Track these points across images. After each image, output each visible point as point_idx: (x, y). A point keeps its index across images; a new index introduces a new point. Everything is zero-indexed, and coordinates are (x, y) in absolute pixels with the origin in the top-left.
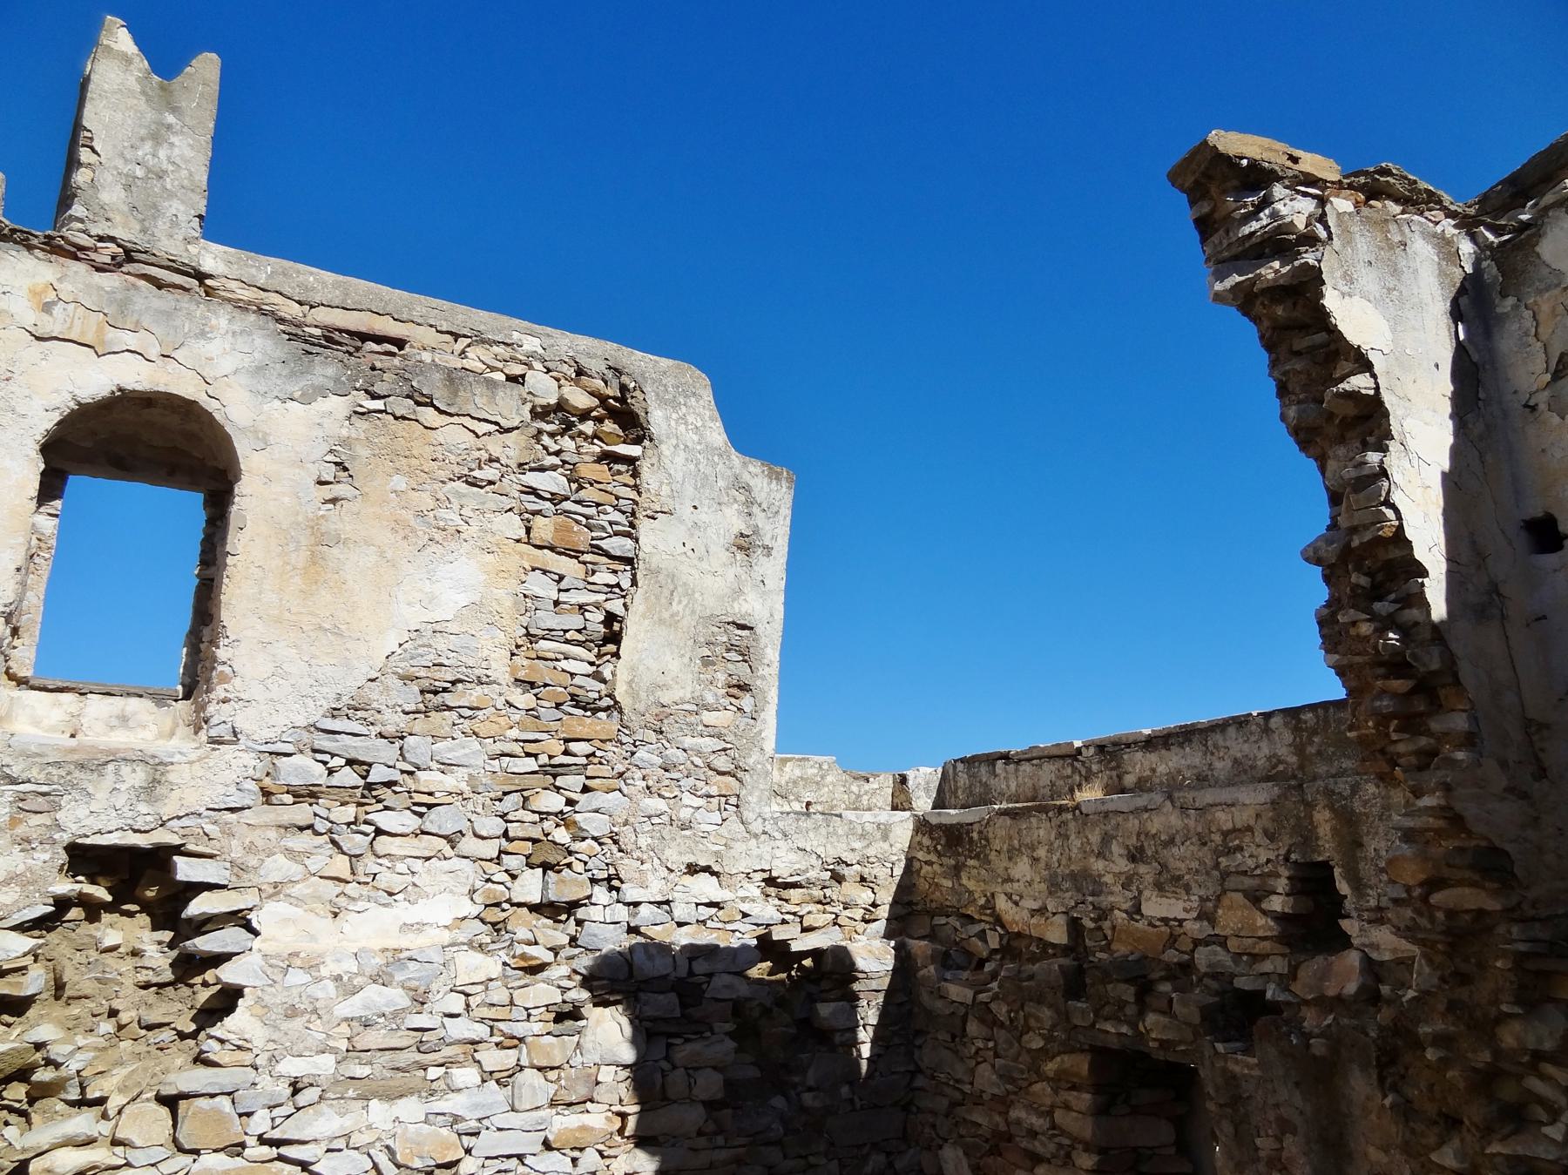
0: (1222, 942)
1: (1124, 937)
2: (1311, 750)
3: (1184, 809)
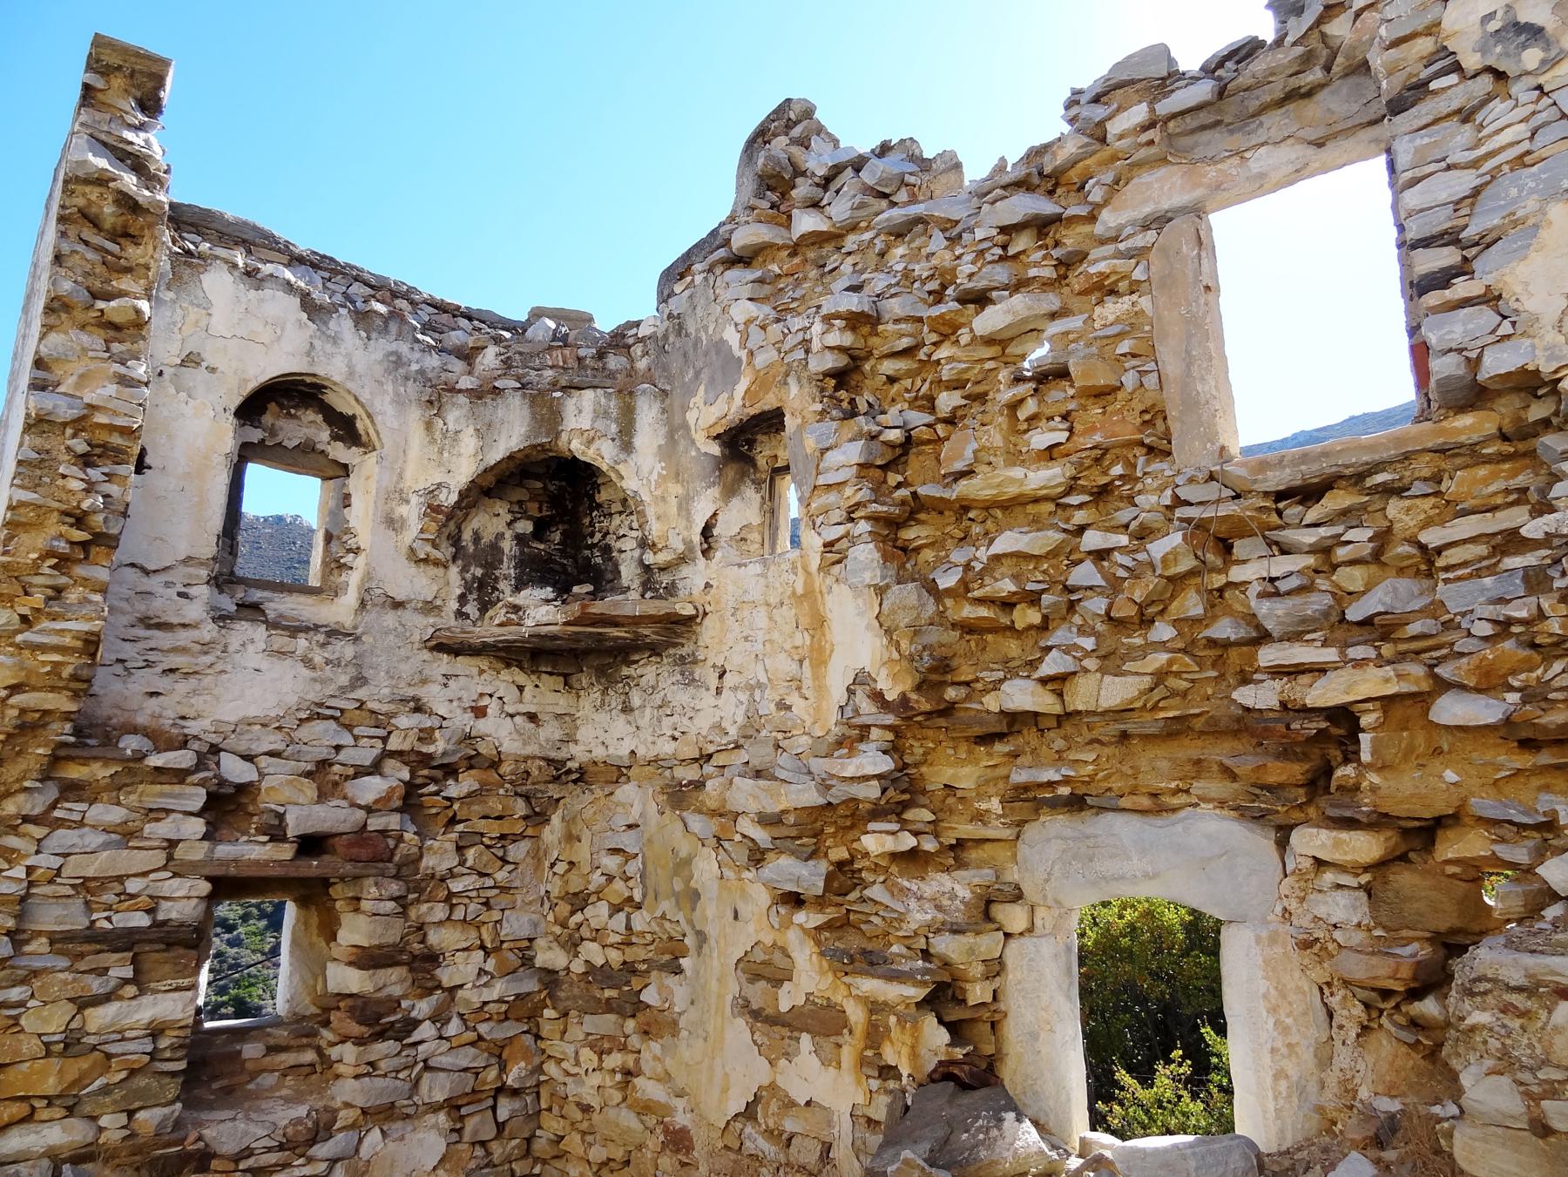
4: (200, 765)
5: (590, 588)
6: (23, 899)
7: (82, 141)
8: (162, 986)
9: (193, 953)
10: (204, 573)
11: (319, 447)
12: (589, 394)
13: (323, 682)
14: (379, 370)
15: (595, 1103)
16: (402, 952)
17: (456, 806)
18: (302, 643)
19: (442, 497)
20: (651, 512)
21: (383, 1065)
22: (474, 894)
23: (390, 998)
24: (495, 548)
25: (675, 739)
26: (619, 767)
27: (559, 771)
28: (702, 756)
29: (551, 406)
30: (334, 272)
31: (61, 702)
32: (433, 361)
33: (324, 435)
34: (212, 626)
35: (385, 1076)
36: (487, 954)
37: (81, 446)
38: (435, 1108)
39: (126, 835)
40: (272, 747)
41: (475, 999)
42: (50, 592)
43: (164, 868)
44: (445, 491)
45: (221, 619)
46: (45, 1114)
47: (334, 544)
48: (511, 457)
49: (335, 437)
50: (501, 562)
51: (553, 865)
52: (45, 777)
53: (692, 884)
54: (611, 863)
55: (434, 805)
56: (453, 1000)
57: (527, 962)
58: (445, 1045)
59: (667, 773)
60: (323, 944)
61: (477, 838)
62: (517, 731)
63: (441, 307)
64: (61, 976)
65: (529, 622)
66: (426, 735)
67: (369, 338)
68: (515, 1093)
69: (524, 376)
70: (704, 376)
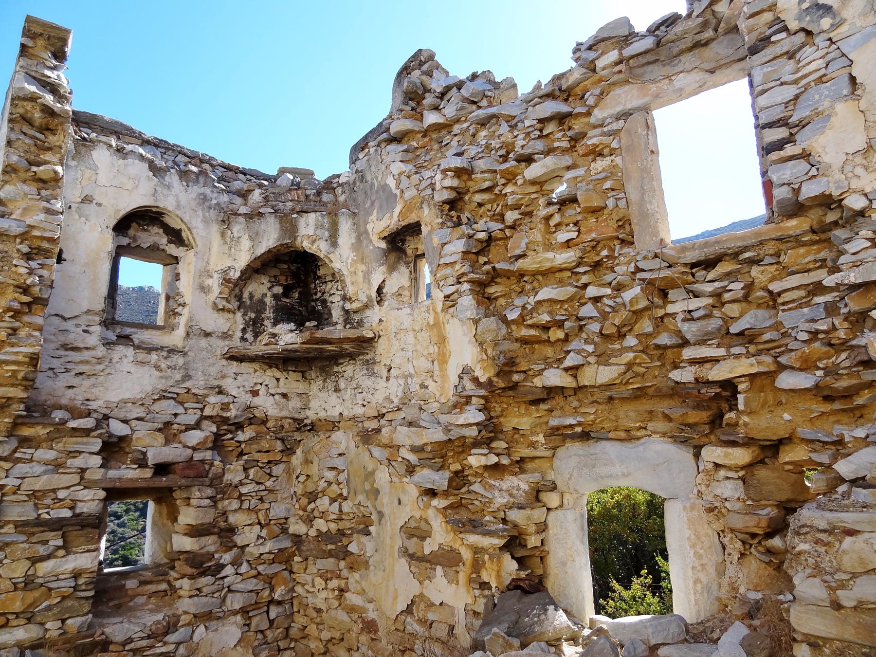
4: (98, 426)
7: (21, 76)
9: (97, 531)
11: (161, 247)
12: (312, 215)
13: (166, 378)
16: (214, 527)
17: (243, 446)
18: (154, 357)
19: (231, 274)
20: (348, 280)
21: (205, 590)
22: (254, 494)
23: (208, 553)
24: (261, 302)
25: (364, 406)
26: (333, 422)
27: (300, 425)
30: (167, 149)
32: (225, 198)
33: (163, 240)
34: (102, 348)
35: (206, 596)
36: (262, 527)
37: (25, 249)
38: (235, 613)
39: (57, 466)
40: (139, 415)
42: (10, 331)
43: (79, 484)
46: (14, 623)
48: (269, 251)
50: (265, 310)
51: (298, 477)
52: (10, 435)
53: (375, 485)
54: (330, 475)
55: (230, 445)
56: (243, 553)
57: (285, 531)
58: (240, 578)
59: (360, 425)
60: (170, 524)
61: (255, 463)
63: (228, 168)
64: (22, 545)
65: (282, 343)
66: (225, 407)
67: (188, 186)
68: (279, 603)
69: (276, 205)
70: (377, 204)
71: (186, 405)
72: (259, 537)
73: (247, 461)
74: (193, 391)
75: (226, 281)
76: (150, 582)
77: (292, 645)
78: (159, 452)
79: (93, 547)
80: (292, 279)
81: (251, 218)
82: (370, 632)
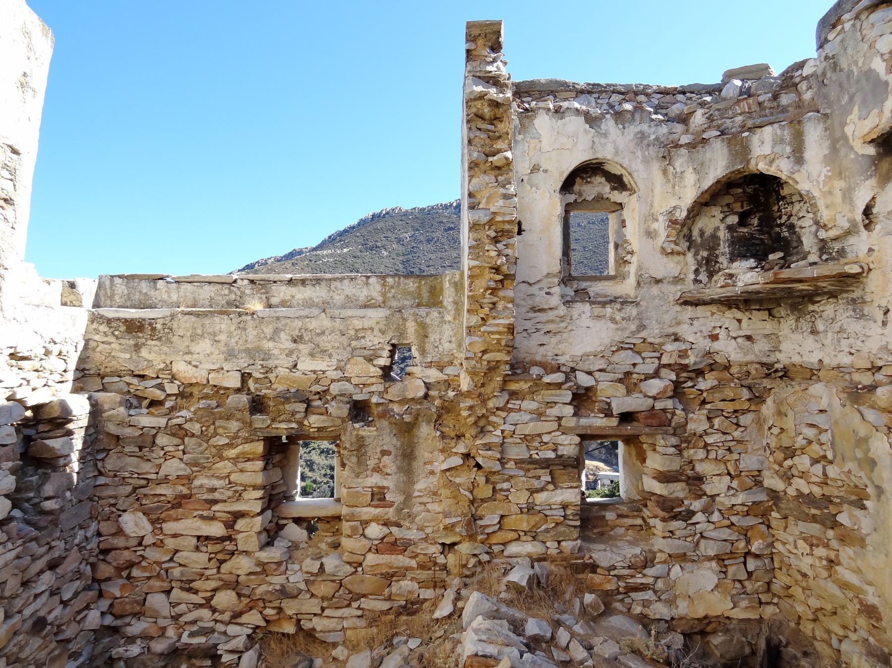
0: (349, 380)
1: (283, 381)
2: (390, 295)
3: (332, 318)
4: (568, 379)
5: (781, 254)
6: (502, 444)
7: (470, 81)
8: (565, 485)
9: (576, 470)
10: (556, 280)
11: (605, 196)
12: (768, 129)
13: (622, 330)
14: (632, 145)
15: (810, 573)
16: (682, 474)
17: (705, 394)
18: (609, 310)
19: (677, 214)
20: (821, 204)
21: (677, 533)
22: (721, 444)
23: (677, 499)
24: (714, 237)
25: (851, 354)
26: (811, 370)
27: (769, 370)
28: (873, 367)
29: (742, 143)
30: (601, 92)
31: (503, 357)
32: (664, 129)
33: (607, 188)
34: (563, 307)
35: (679, 538)
36: (732, 478)
37: (493, 234)
38: (710, 559)
39: (539, 415)
40: (600, 367)
41: (727, 503)
42: (491, 306)
43: (558, 430)
44: (678, 210)
45: (567, 303)
46: (524, 538)
47: (620, 249)
48: (718, 182)
49: (613, 189)
50: (719, 245)
51: (770, 428)
52: (502, 390)
53: (870, 455)
54: (810, 433)
55: (692, 393)
56: (714, 501)
57: (758, 483)
58: (712, 526)
59: (847, 377)
60: (640, 464)
61: (720, 413)
62: (740, 347)
63: (664, 92)
64: (522, 479)
65: (740, 284)
66: (683, 354)
67: (624, 128)
68: (757, 556)
69: (722, 124)
70: (858, 98)
71: (643, 355)
72: (729, 488)
73: (710, 411)
74: (649, 340)
75: (673, 223)
76: (626, 516)
77: (775, 600)
78: (622, 403)
79: (575, 484)
80: (749, 204)
81: (694, 148)
82: (871, 618)
